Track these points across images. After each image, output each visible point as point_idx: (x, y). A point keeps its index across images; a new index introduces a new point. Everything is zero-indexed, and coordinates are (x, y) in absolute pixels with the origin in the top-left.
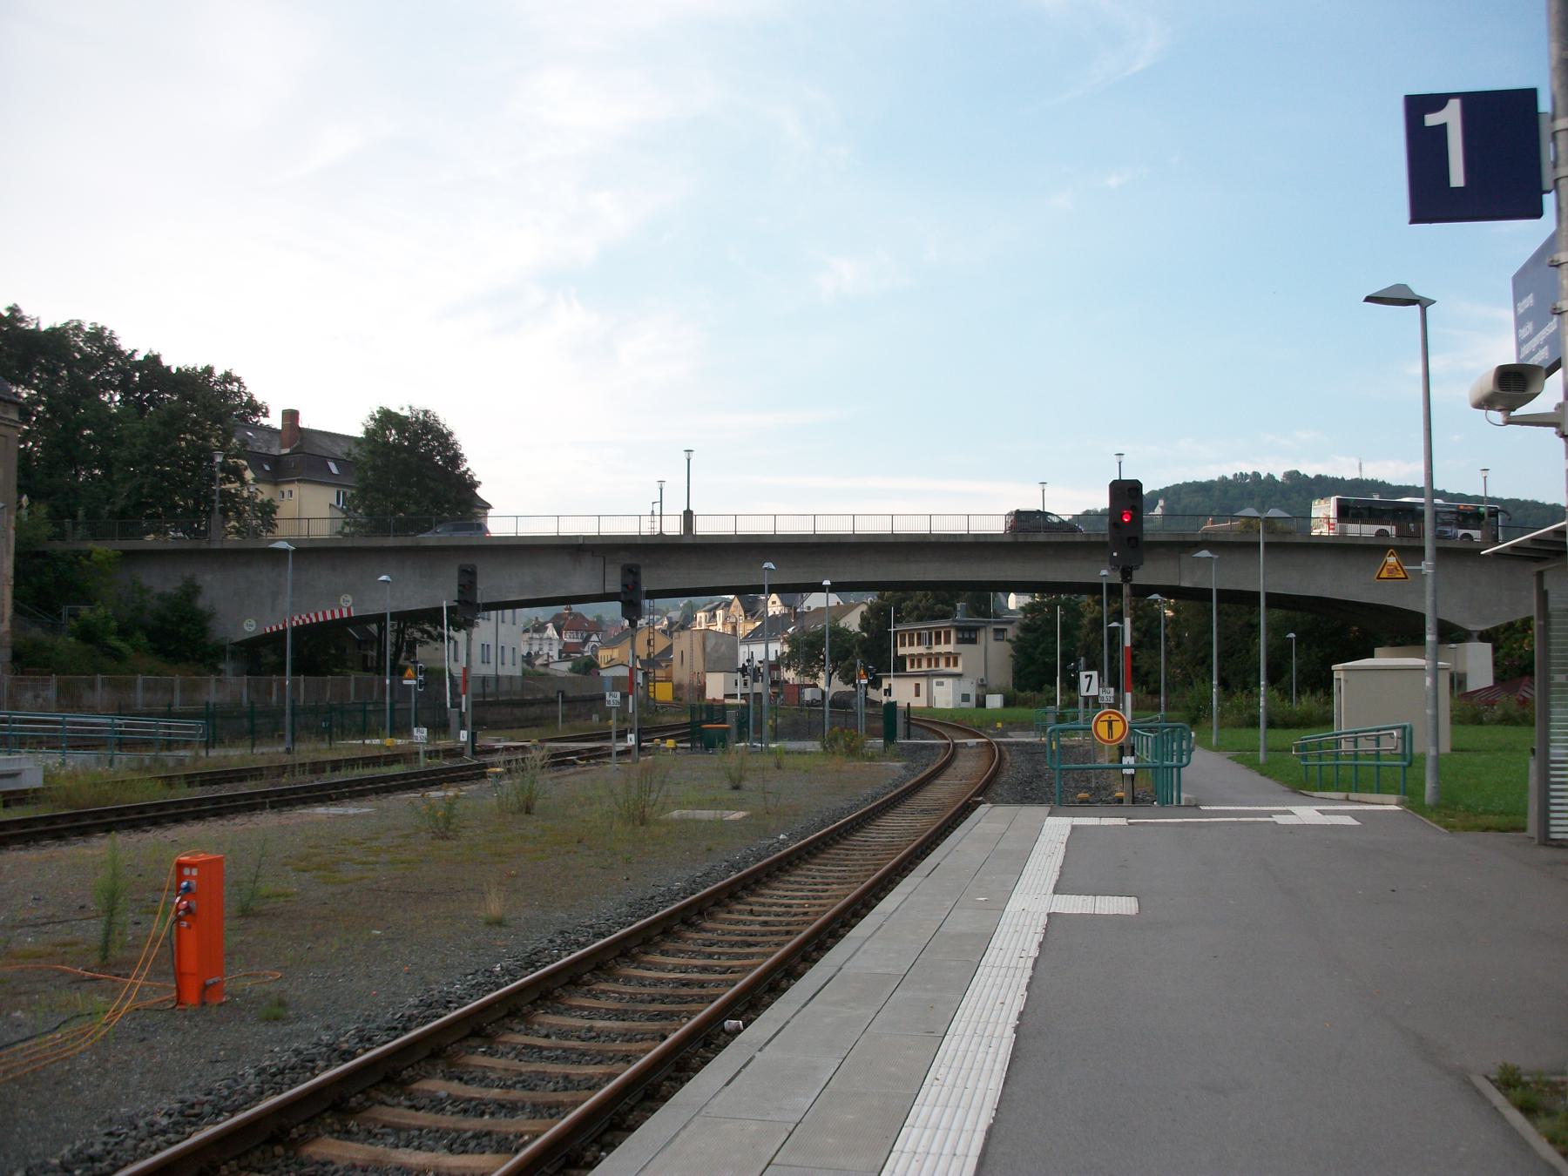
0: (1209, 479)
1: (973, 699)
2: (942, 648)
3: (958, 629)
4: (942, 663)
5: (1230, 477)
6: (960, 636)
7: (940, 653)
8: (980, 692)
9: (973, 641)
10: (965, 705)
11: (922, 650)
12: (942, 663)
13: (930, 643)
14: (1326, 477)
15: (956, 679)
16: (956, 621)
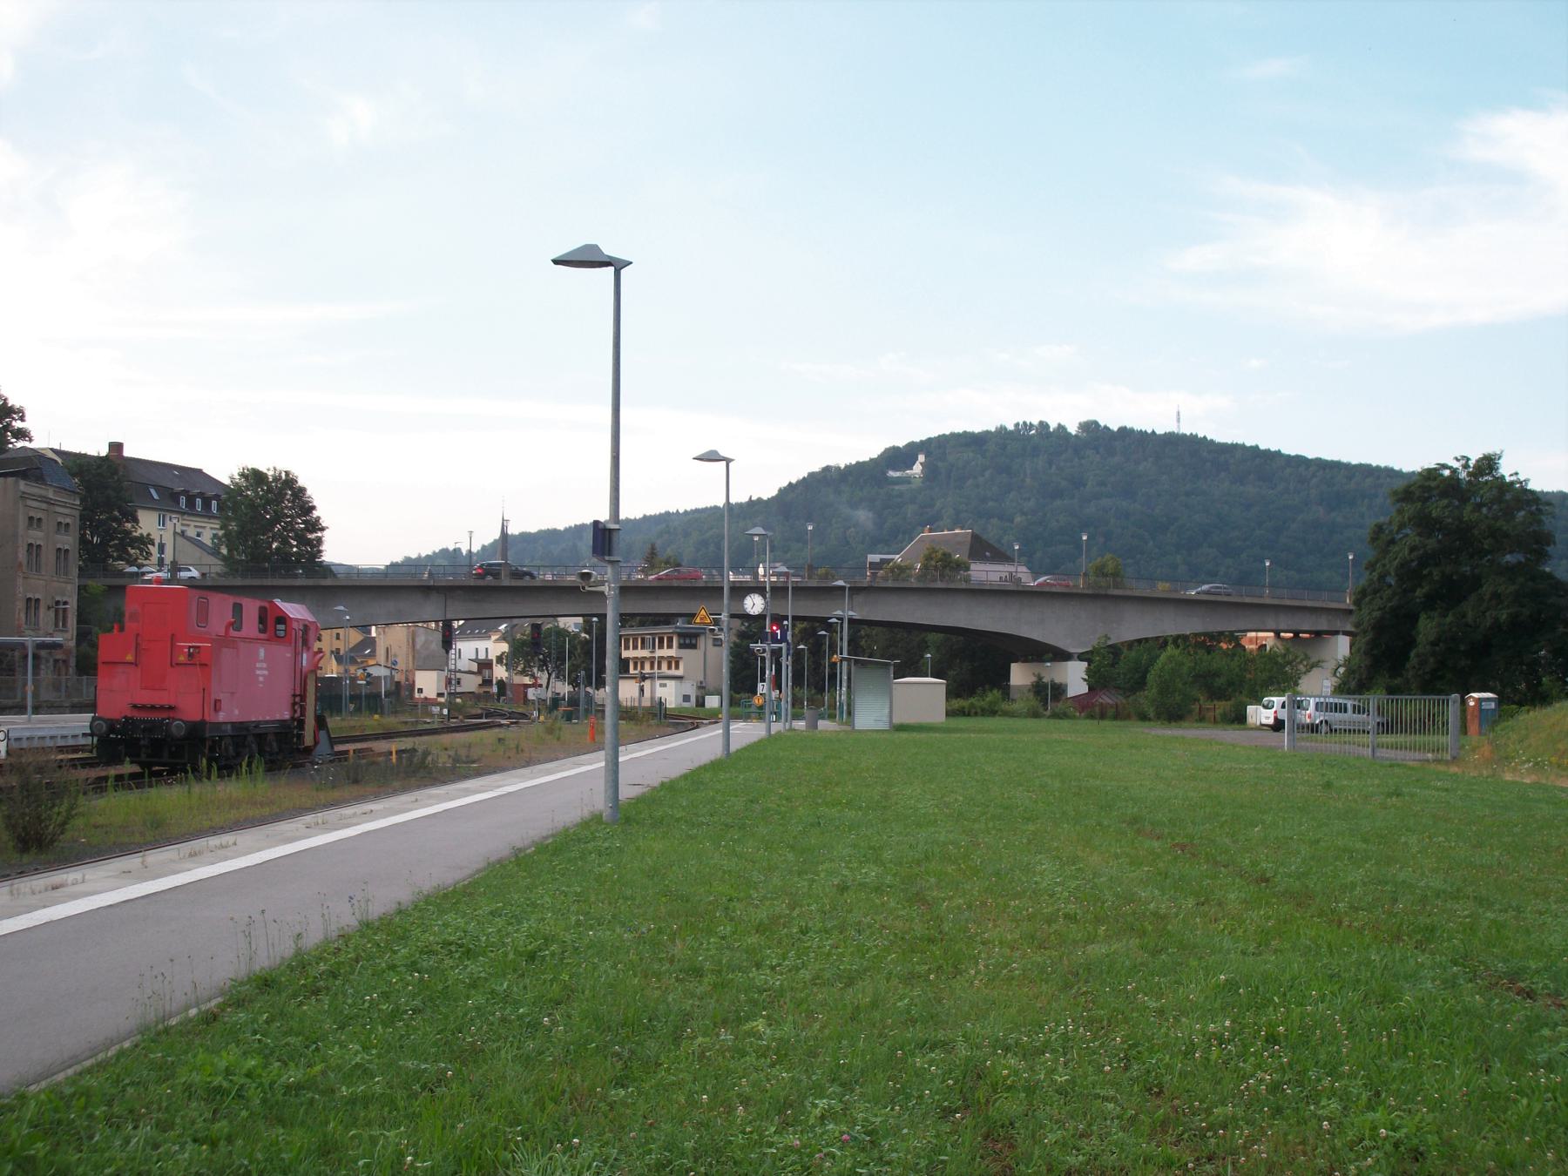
0: (985, 429)
1: (693, 699)
2: (665, 652)
3: (680, 635)
4: (664, 665)
5: (1011, 427)
6: (682, 641)
7: (662, 657)
8: (699, 694)
9: (694, 646)
10: (686, 705)
11: (645, 653)
12: (664, 665)
13: (654, 647)
14: (1132, 430)
15: (678, 682)
16: (676, 628)
